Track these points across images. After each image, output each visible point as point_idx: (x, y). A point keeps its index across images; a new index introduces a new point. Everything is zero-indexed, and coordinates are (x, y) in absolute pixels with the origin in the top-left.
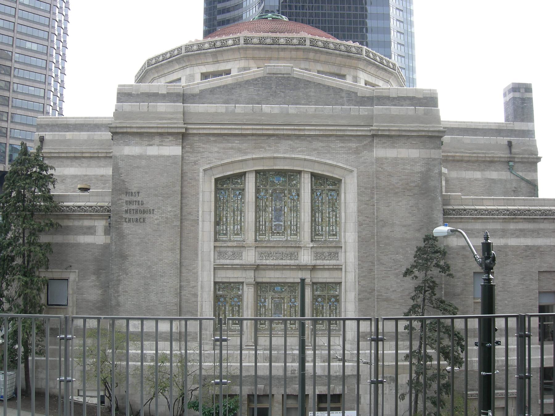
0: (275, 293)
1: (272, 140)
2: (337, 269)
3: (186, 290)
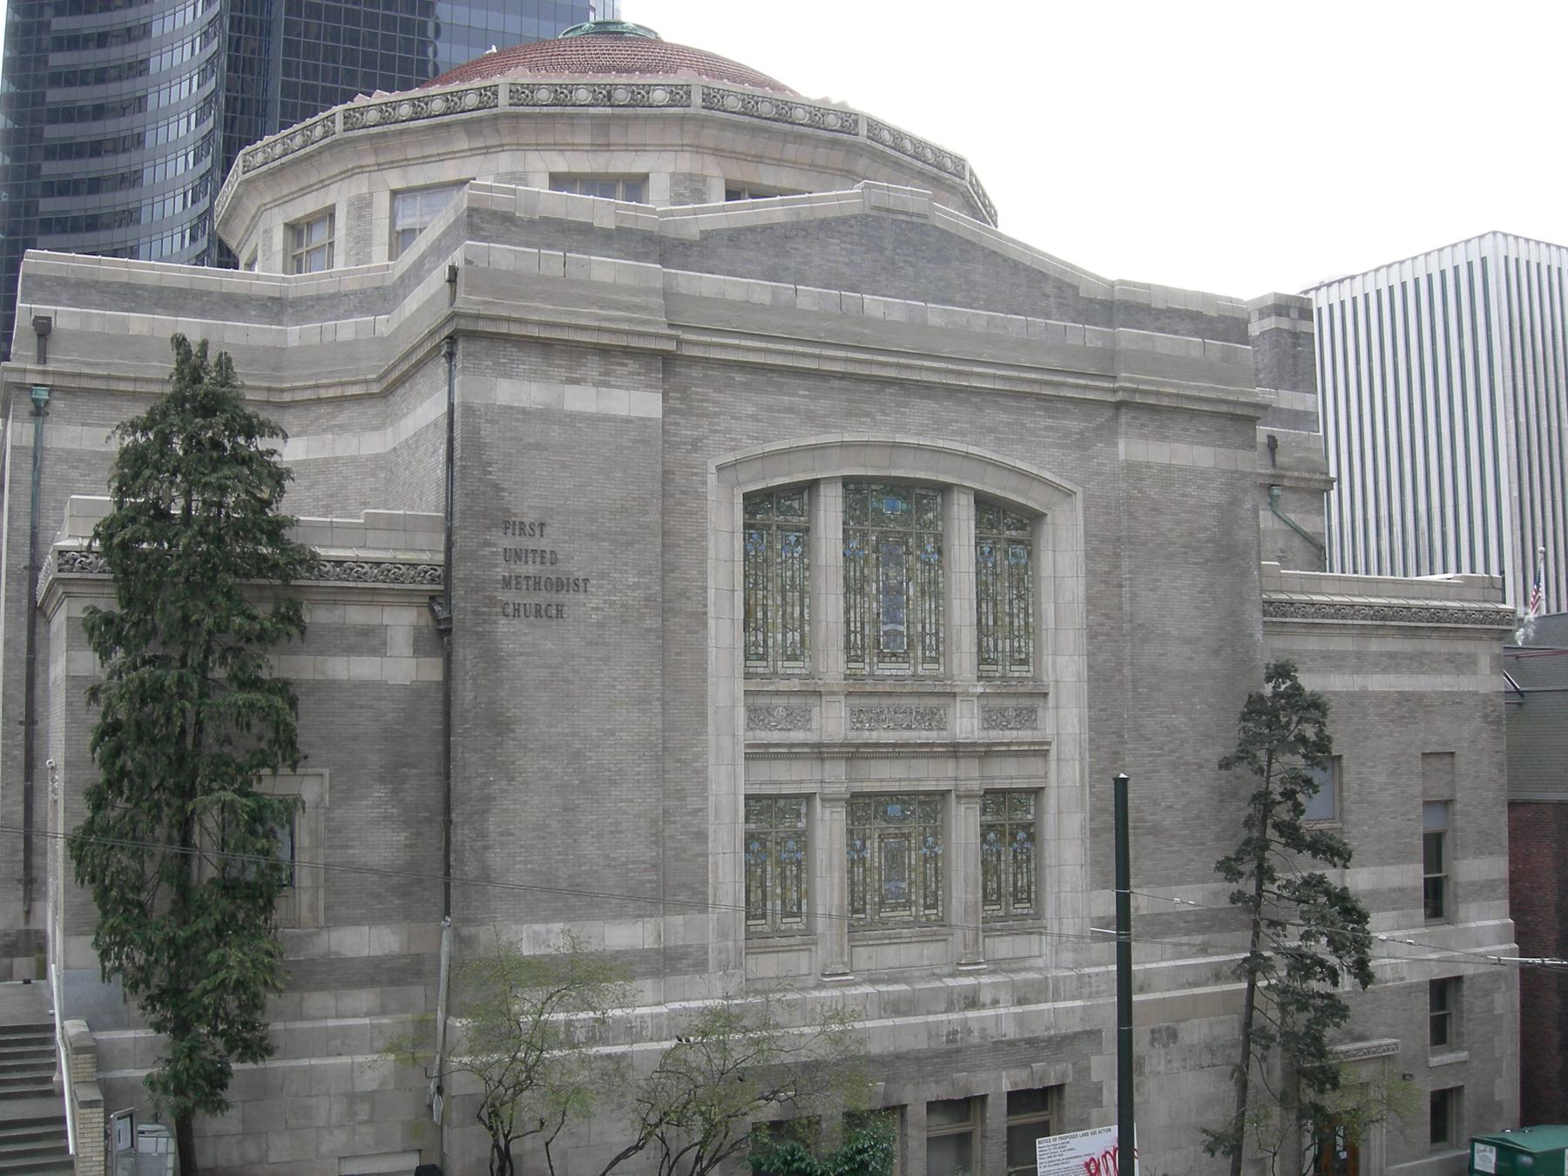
0: (888, 822)
1: (891, 394)
2: (1035, 753)
3: (674, 822)
